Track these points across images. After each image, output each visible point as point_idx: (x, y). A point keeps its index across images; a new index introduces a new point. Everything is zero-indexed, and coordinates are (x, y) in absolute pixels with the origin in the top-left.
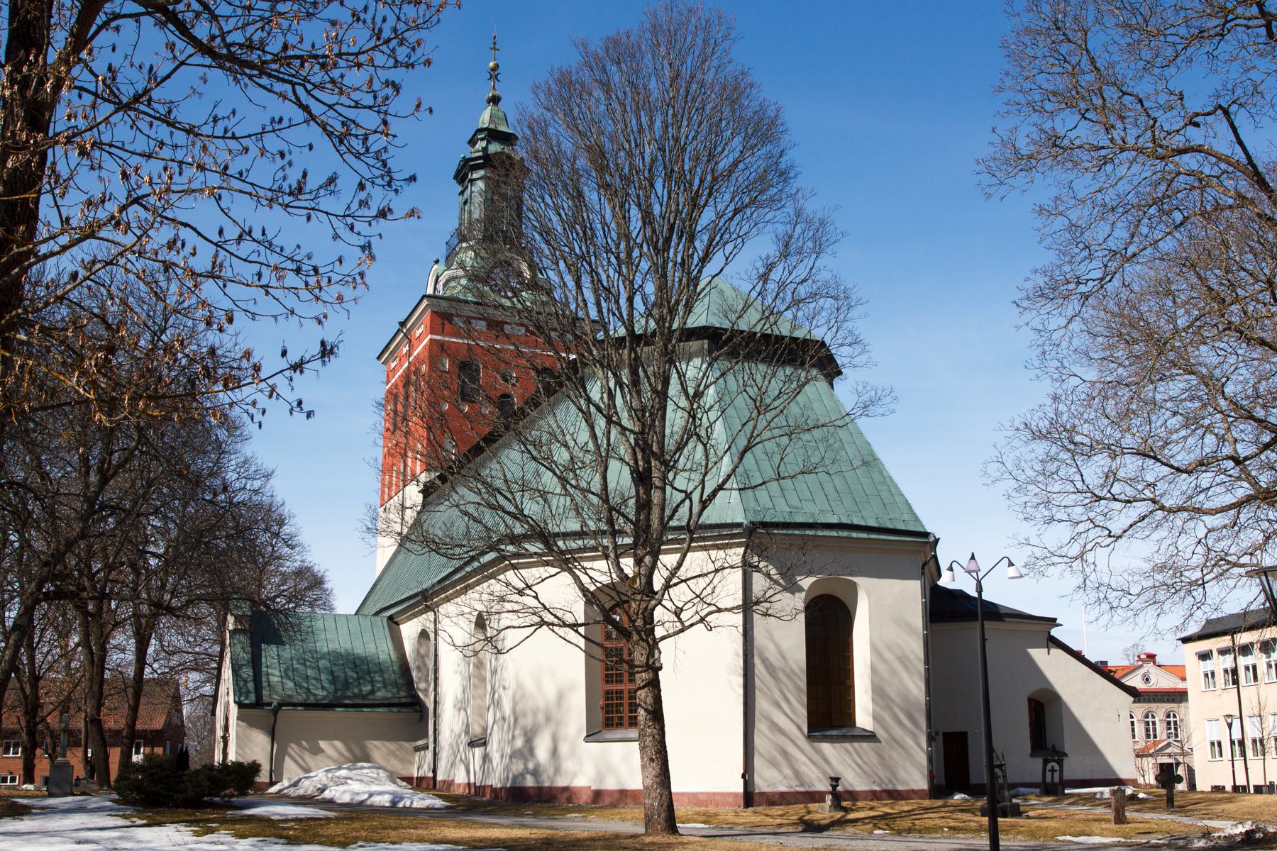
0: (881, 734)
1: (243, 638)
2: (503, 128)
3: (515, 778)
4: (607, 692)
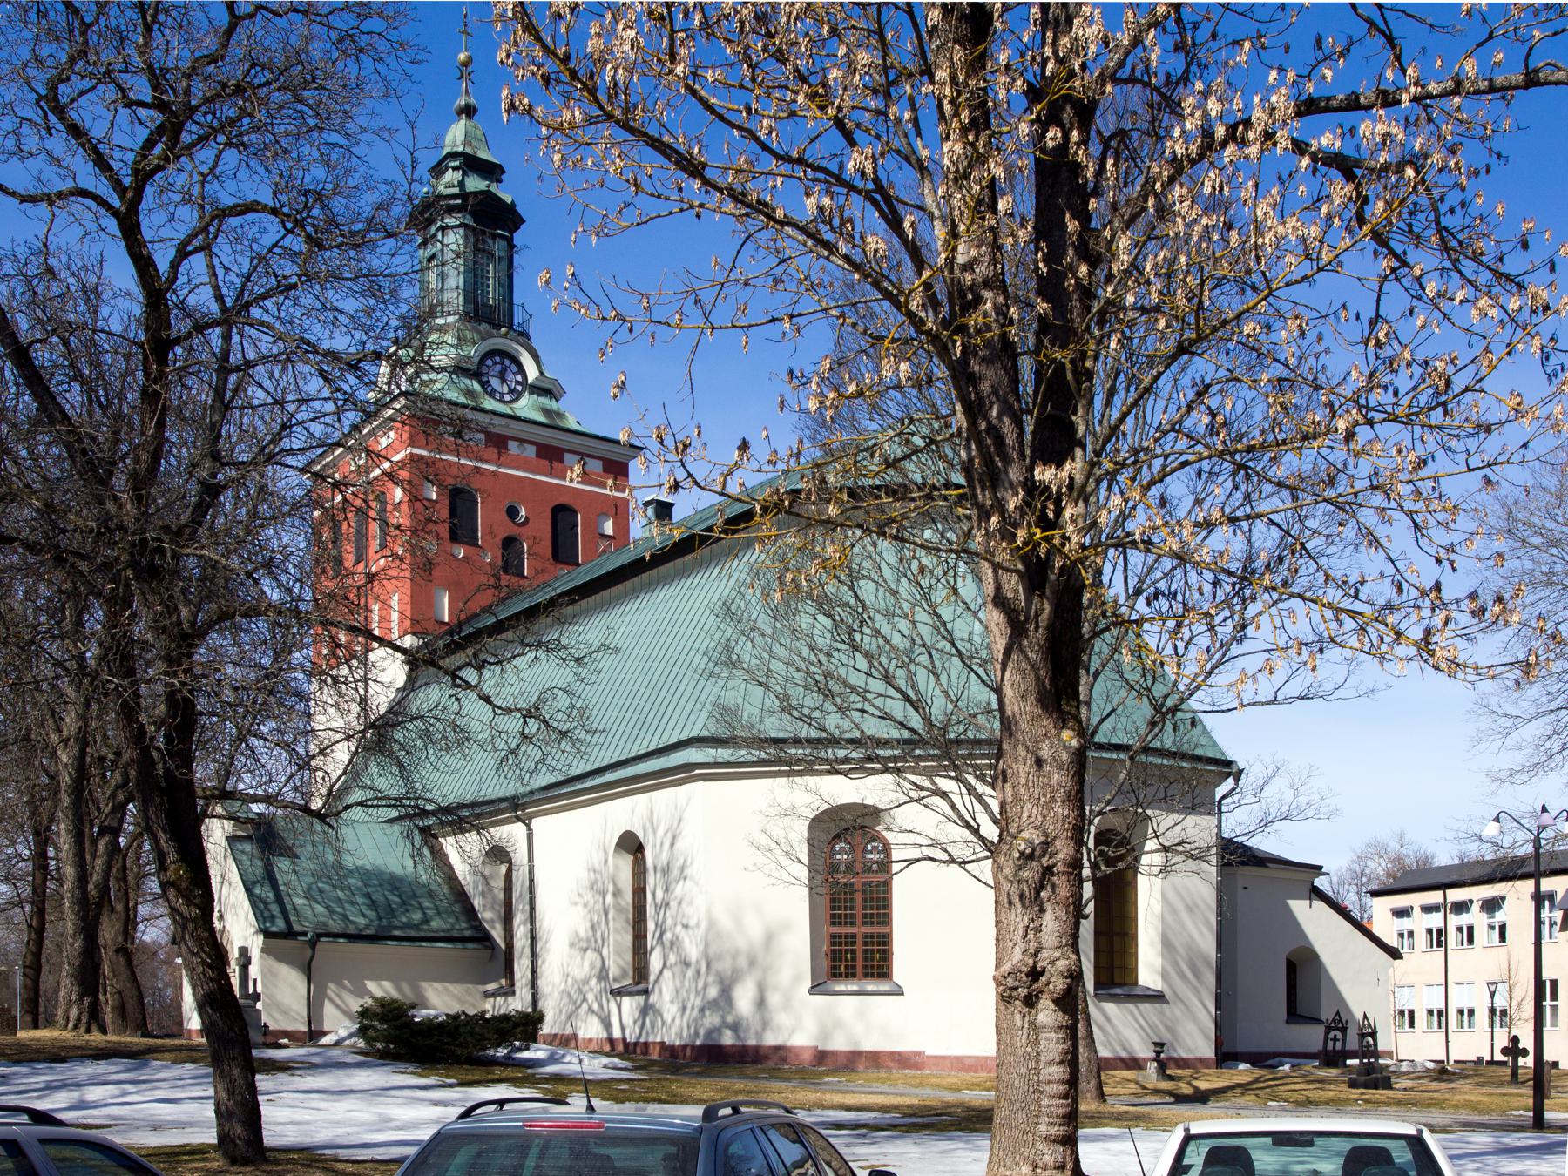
0: (1168, 994)
1: (248, 847)
2: (483, 154)
3: (709, 1033)
4: (833, 936)
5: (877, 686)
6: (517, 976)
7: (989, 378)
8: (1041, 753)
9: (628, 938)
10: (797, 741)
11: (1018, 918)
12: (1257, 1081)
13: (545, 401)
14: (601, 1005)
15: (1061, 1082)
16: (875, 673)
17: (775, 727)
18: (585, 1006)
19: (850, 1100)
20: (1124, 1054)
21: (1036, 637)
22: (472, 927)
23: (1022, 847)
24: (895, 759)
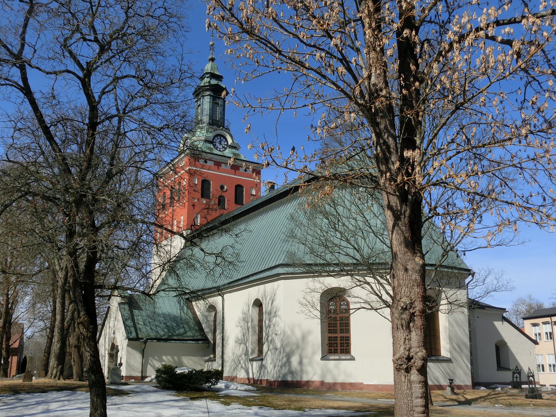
2: (217, 73)
4: (329, 337)
5: (344, 244)
6: (217, 354)
7: (383, 124)
8: (408, 267)
9: (256, 337)
10: (316, 265)
11: (402, 334)
12: (489, 395)
13: (234, 150)
14: (245, 365)
15: (422, 406)
16: (343, 239)
17: (308, 259)
18: (240, 366)
19: (336, 404)
20: (437, 384)
21: (405, 220)
22: (202, 335)
23: (402, 305)
24: (351, 270)
